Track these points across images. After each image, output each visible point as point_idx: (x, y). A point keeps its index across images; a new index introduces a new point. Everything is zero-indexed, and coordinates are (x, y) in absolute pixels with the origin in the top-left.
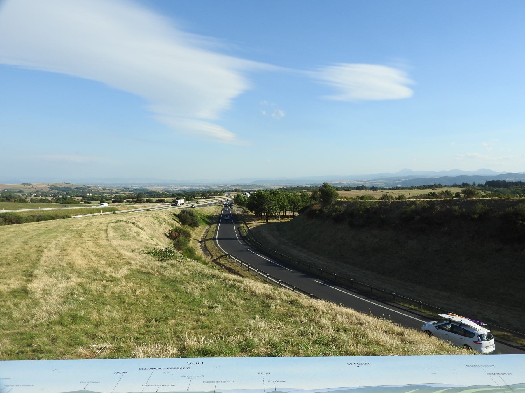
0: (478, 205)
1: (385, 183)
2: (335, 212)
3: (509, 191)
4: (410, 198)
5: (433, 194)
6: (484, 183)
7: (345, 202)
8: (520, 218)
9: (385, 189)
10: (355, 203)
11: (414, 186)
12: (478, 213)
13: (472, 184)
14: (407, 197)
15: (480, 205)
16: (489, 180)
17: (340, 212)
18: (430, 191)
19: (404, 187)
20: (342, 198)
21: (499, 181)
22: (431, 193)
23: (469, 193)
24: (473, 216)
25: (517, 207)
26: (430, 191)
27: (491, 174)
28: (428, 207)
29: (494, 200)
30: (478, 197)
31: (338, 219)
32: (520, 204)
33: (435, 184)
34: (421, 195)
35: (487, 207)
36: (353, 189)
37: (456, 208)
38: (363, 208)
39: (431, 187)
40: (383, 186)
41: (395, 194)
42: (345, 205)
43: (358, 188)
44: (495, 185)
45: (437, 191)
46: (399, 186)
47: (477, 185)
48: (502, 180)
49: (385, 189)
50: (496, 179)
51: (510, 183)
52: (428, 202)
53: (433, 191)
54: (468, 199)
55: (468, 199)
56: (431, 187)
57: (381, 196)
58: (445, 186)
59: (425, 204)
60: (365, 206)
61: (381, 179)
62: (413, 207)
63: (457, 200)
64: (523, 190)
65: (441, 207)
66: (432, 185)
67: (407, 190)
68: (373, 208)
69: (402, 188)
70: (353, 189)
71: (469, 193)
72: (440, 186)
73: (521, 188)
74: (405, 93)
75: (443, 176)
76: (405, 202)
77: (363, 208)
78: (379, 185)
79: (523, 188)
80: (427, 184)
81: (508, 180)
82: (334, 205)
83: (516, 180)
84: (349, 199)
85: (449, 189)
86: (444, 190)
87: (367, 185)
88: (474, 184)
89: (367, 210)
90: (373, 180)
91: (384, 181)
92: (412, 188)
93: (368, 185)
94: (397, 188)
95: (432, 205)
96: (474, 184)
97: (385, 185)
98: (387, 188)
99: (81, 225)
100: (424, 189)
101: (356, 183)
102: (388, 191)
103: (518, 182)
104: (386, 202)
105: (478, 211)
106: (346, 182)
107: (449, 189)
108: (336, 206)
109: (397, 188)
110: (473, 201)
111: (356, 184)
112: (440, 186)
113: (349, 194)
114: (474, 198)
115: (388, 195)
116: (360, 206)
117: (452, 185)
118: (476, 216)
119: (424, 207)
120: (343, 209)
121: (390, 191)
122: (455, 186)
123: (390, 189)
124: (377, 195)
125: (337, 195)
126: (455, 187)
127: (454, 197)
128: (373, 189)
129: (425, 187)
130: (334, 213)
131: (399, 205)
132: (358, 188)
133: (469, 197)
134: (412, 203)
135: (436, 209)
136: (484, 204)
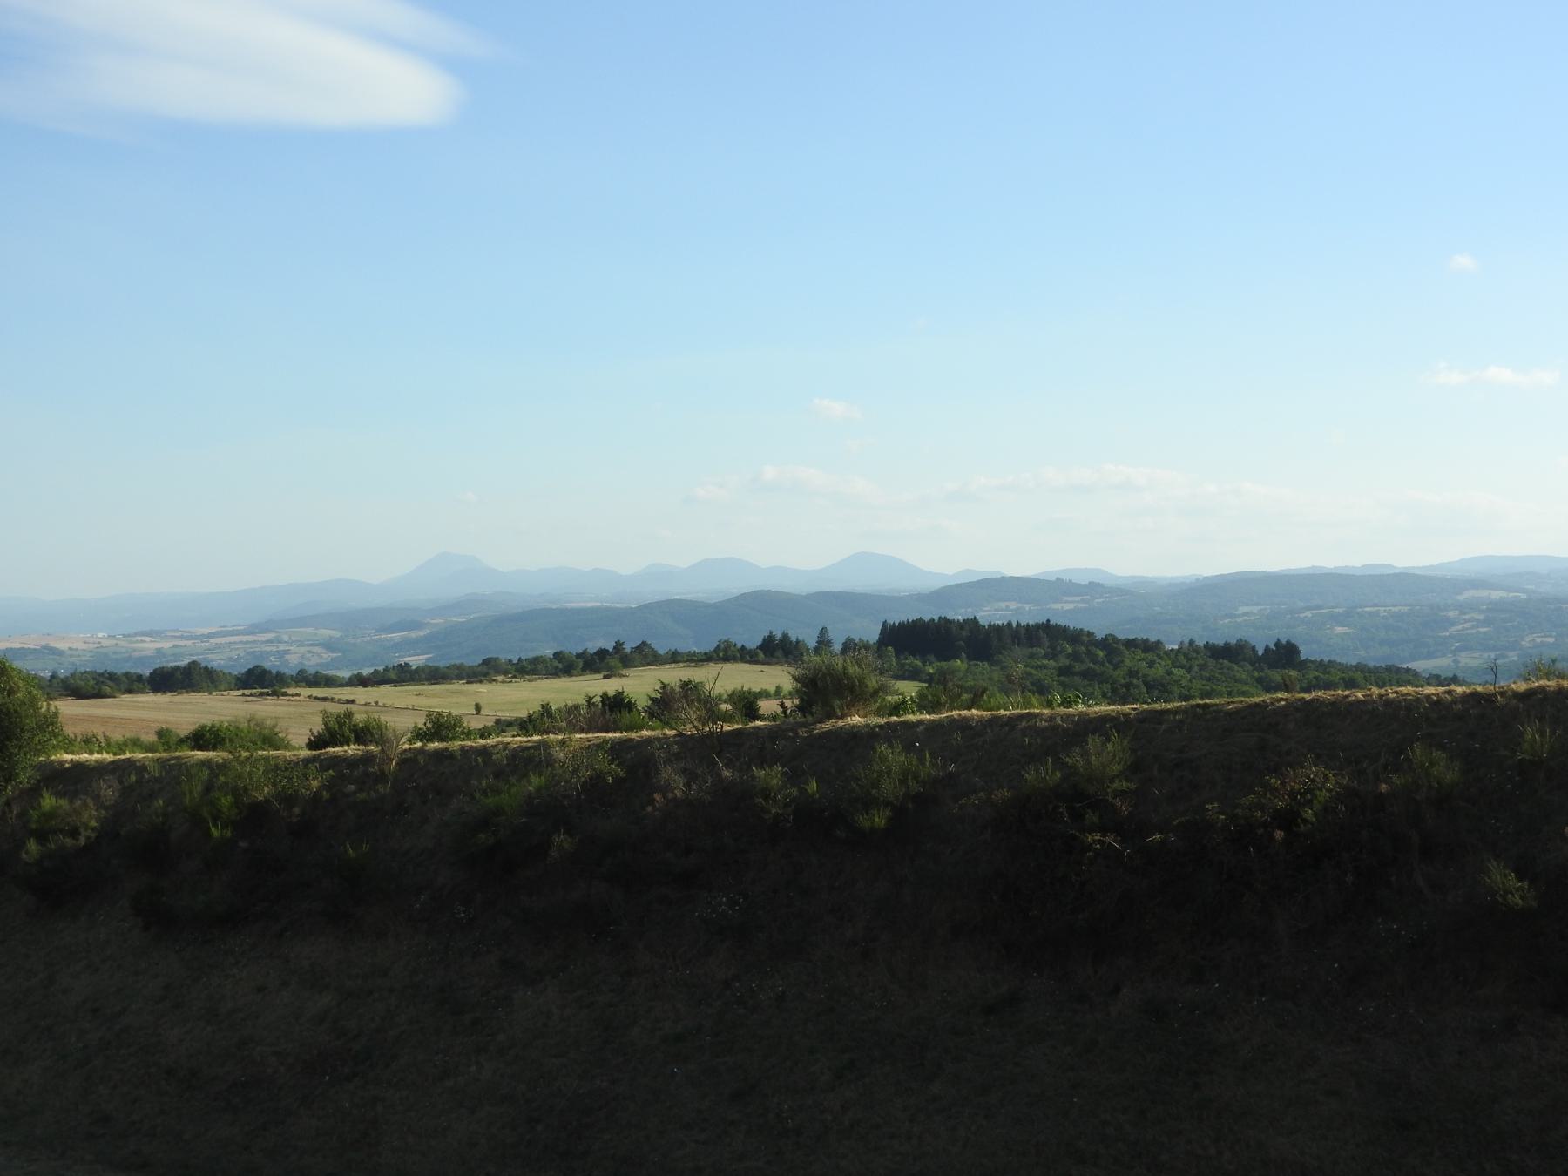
0: (883, 759)
1: (329, 645)
2: (41, 836)
3: (997, 675)
4: (484, 733)
5: (617, 705)
6: (872, 634)
7: (101, 769)
8: (1092, 817)
9: (329, 682)
10: (173, 772)
11: (503, 657)
12: (887, 804)
13: (812, 643)
14: (476, 724)
15: (893, 757)
16: (897, 617)
17: (74, 833)
18: (595, 686)
19: (442, 664)
20: (88, 743)
21: (945, 623)
22: (605, 697)
23: (823, 688)
24: (863, 821)
25: (1074, 758)
26: (595, 686)
27: (903, 584)
28: (619, 781)
29: (963, 725)
30: (878, 713)
31: (64, 884)
32: (1093, 742)
33: (619, 646)
34: (546, 710)
35: (929, 768)
36: (132, 684)
37: (770, 776)
38: (226, 801)
39: (596, 662)
40: (315, 661)
41: (401, 712)
42: (108, 791)
43: (167, 680)
44: (930, 641)
45: (640, 685)
46: (416, 661)
47: (837, 647)
48: (958, 615)
49: (329, 682)
50: (929, 614)
51: (997, 630)
52: (617, 749)
53: (611, 686)
54: (829, 725)
55: (829, 725)
56: (596, 662)
57: (318, 727)
58: (674, 658)
59: (602, 762)
60: (235, 792)
61: (302, 621)
62: (536, 781)
63: (734, 743)
64: (1064, 671)
65: (691, 777)
66: (602, 653)
67: (459, 686)
68: (289, 799)
69: (434, 676)
70: (132, 684)
71: (823, 688)
72: (644, 656)
73: (1054, 657)
74: (402, 90)
75: (657, 598)
76: (485, 752)
77: (226, 801)
78: (294, 659)
79: (1064, 661)
80: (573, 648)
81: (991, 614)
82: (34, 792)
83: (1028, 614)
84: (121, 748)
85: (698, 674)
86: (674, 675)
87: (216, 661)
88: (824, 642)
89: (254, 817)
90: (253, 629)
91: (325, 633)
92: (487, 670)
93: (227, 657)
94: (403, 676)
95: (638, 763)
96: (824, 642)
97: (327, 656)
98: (345, 674)
99: (1007, 608)
100: (555, 673)
101: (149, 646)
102: (347, 693)
103: (1038, 627)
104: (368, 759)
105: (888, 788)
106: (81, 644)
107: (698, 674)
108: (48, 801)
109: (403, 676)
110: (854, 734)
111: (152, 651)
112: (644, 656)
113: (104, 721)
114: (857, 720)
115: (359, 718)
116: (208, 788)
117: (709, 647)
118: (879, 819)
119: (598, 778)
120: (91, 818)
121: (360, 694)
122: (726, 653)
123: (362, 681)
124: (296, 721)
125: (50, 723)
126: (727, 659)
127: (727, 718)
128: (259, 680)
129: (564, 666)
130: (33, 846)
131: (443, 772)
132: (167, 680)
133: (831, 715)
134: (523, 761)
135: (665, 789)
136: (909, 748)
